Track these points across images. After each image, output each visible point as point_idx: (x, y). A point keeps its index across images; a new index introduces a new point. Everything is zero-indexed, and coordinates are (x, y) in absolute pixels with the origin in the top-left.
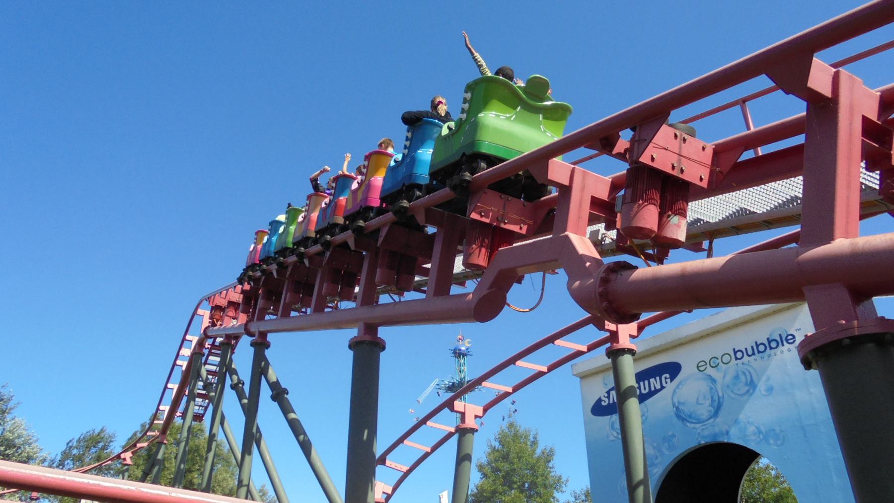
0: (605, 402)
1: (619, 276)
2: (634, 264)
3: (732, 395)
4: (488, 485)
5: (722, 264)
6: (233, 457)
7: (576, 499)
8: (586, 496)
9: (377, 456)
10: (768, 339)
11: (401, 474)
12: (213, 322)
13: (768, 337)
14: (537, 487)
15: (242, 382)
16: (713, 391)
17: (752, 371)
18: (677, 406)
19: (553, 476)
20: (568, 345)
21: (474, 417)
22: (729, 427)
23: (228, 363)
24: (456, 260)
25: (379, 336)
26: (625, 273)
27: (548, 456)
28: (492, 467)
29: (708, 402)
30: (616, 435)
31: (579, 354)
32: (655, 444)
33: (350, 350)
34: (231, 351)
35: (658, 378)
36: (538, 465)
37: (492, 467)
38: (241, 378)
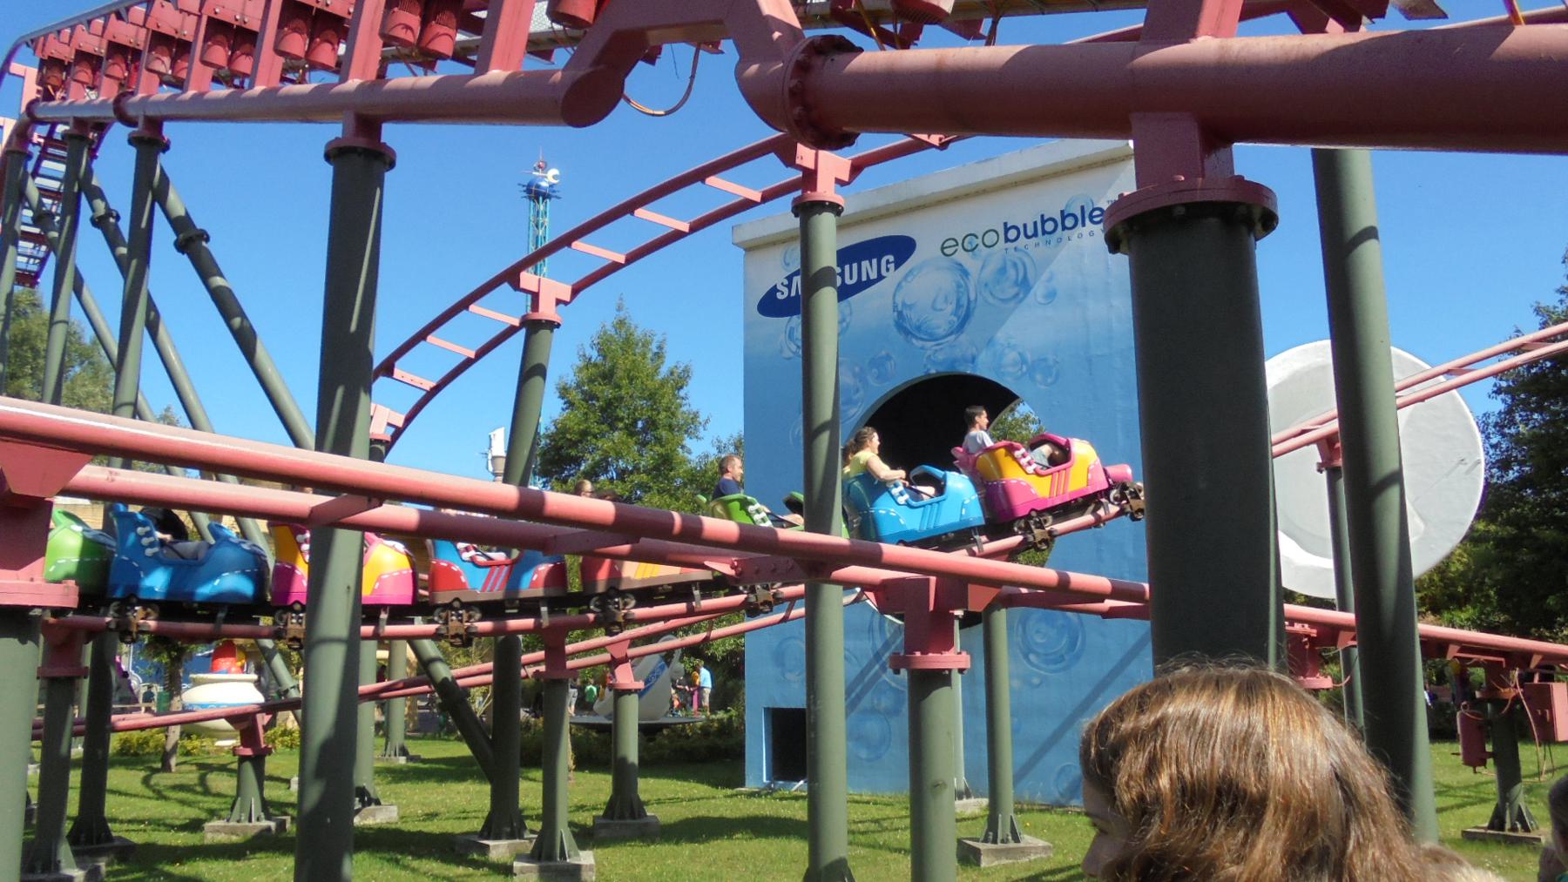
0: (783, 293)
1: (829, 61)
3: (991, 300)
4: (575, 421)
5: (1008, 59)
6: (103, 352)
7: (720, 452)
8: (737, 448)
12: (46, 90)
15: (114, 214)
16: (962, 290)
17: (1026, 260)
19: (684, 413)
20: (729, 187)
22: (977, 349)
23: (85, 173)
25: (382, 141)
26: (839, 58)
27: (679, 380)
28: (583, 392)
29: (951, 308)
30: (794, 349)
31: (747, 204)
32: (857, 369)
33: (327, 164)
34: (88, 153)
35: (875, 261)
36: (661, 392)
37: (583, 392)
38: (112, 207)
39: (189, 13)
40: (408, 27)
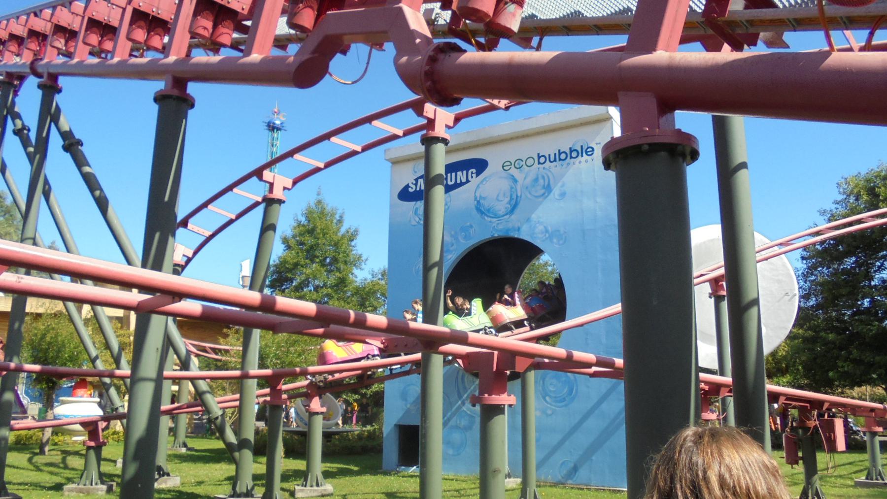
0: (412, 188)
1: (447, 56)
2: (464, 48)
3: (529, 196)
4: (291, 257)
7: (373, 277)
8: (383, 275)
9: (179, 219)
10: (570, 148)
11: (203, 239)
13: (571, 146)
14: (338, 263)
15: (27, 128)
16: (513, 190)
17: (551, 177)
18: (478, 199)
19: (353, 254)
20: (384, 127)
21: (282, 188)
24: (279, 21)
26: (454, 55)
27: (352, 236)
29: (508, 199)
30: (419, 220)
31: (394, 137)
32: (453, 233)
35: (465, 172)
39: (77, 15)
40: (205, 28)
